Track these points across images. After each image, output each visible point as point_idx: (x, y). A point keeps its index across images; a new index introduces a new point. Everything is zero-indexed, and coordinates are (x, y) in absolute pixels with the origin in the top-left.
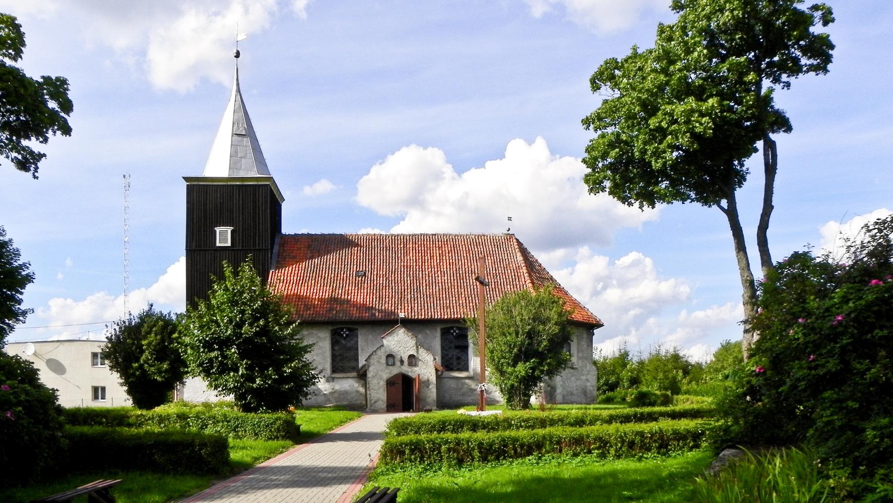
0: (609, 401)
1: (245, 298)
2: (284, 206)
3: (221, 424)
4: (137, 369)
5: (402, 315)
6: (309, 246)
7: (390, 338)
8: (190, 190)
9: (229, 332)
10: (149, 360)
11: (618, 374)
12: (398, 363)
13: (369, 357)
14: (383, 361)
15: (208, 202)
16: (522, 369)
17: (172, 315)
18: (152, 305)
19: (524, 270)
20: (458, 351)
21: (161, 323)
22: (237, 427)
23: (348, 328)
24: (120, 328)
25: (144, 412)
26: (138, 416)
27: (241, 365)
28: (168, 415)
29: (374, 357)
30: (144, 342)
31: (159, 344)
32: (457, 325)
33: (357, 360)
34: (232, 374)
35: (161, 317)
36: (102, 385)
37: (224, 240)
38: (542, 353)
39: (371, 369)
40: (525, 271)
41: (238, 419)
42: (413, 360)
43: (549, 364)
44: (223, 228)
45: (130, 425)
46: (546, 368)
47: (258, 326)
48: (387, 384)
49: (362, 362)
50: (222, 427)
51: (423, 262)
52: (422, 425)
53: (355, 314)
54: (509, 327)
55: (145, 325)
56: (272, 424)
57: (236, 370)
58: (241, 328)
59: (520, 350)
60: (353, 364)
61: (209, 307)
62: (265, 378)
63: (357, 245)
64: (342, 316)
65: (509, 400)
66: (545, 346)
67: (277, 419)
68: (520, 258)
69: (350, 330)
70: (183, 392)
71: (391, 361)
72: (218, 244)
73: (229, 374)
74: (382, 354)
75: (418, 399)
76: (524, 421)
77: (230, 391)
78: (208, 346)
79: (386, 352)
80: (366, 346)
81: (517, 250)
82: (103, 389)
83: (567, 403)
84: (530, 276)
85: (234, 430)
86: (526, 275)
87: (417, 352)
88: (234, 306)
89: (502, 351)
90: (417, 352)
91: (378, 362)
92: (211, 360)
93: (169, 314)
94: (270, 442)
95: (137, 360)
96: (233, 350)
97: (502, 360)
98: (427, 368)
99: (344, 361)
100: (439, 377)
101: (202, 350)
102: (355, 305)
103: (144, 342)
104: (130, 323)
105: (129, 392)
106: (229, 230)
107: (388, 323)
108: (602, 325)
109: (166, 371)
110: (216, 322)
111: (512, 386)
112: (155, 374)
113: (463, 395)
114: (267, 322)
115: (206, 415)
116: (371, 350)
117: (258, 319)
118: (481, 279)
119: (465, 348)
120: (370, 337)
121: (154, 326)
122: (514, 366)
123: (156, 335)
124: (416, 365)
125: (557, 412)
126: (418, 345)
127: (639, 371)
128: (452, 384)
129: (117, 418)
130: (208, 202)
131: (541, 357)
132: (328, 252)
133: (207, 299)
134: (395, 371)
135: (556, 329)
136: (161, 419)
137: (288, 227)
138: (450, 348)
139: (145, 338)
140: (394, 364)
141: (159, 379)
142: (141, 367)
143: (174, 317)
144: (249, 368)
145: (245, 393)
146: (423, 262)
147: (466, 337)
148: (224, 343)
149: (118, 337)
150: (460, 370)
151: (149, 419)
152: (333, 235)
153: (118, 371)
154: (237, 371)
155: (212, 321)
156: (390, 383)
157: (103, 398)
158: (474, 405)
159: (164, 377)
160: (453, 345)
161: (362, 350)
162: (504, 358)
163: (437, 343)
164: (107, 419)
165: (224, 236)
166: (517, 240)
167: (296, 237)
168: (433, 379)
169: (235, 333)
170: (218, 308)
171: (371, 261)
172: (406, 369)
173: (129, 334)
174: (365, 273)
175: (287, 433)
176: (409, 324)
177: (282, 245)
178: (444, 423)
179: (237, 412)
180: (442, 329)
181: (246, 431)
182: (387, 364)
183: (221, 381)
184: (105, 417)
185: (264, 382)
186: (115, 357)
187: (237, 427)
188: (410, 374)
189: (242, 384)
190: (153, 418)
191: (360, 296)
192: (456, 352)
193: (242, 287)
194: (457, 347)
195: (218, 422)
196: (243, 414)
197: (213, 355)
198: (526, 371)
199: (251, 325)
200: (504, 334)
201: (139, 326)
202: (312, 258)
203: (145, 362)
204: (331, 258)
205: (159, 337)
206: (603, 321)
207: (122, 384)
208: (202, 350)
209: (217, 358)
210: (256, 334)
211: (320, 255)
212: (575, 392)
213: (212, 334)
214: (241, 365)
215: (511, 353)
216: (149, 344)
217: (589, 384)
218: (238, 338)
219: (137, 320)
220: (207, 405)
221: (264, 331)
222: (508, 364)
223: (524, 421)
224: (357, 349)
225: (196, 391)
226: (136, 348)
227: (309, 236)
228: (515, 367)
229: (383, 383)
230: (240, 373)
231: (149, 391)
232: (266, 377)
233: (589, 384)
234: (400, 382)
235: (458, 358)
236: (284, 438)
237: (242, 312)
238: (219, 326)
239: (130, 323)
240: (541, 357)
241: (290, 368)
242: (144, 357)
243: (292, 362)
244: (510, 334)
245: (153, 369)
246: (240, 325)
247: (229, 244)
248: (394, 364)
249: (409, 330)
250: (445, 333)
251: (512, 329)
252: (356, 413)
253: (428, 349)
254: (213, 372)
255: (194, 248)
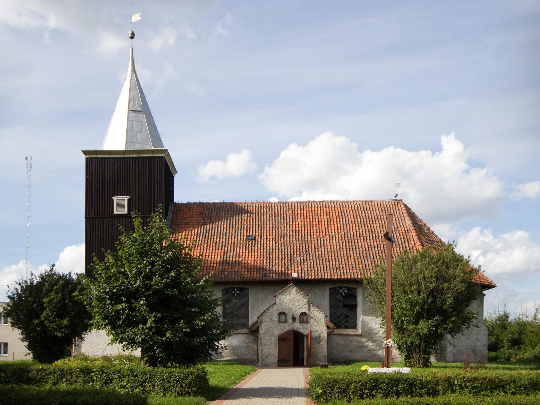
0: (492, 360)
1: (155, 249)
2: (177, 178)
3: (127, 379)
4: (37, 325)
5: (295, 275)
6: (201, 214)
7: (282, 297)
8: (89, 162)
9: (138, 284)
10: (49, 316)
11: (498, 336)
12: (290, 321)
13: (262, 314)
14: (276, 318)
15: (105, 174)
16: (423, 326)
17: (72, 274)
18: (53, 266)
19: (414, 233)
20: (346, 309)
21: (61, 282)
22: (145, 381)
23: (243, 285)
24: (22, 287)
25: (45, 366)
26: (39, 370)
27: (150, 317)
28: (71, 369)
29: (267, 314)
30: (45, 300)
31: (60, 301)
32: (347, 285)
33: (247, 318)
34: (140, 326)
35: (63, 278)
36: (5, 341)
37: (120, 208)
38: (445, 311)
39: (263, 325)
40: (414, 234)
41: (145, 373)
42: (304, 317)
43: (453, 322)
44: (120, 198)
45: (29, 381)
46: (451, 325)
47: (168, 278)
48: (279, 340)
49: (252, 319)
50: (128, 382)
51: (312, 227)
52: (352, 383)
53: (247, 276)
54: (411, 285)
55: (46, 284)
56: (183, 379)
57: (145, 322)
58: (151, 280)
59: (422, 308)
60: (243, 321)
61: (117, 258)
62: (175, 331)
63: (247, 212)
64: (234, 277)
65: (407, 358)
66: (450, 304)
67: (188, 374)
68: (408, 222)
69: (240, 289)
70: (81, 347)
71: (283, 318)
72: (115, 212)
73: (138, 326)
74: (274, 312)
75: (309, 354)
76: (469, 381)
77: (138, 344)
78: (115, 298)
79: (278, 310)
80: (257, 306)
81: (405, 215)
82: (6, 345)
83: (456, 362)
84: (419, 238)
85: (142, 385)
86: (416, 238)
87: (309, 310)
88: (143, 257)
89: (402, 308)
90: (309, 310)
91: (271, 319)
92: (118, 312)
93: (70, 274)
94: (181, 398)
95: (38, 317)
96: (142, 302)
97: (403, 318)
98: (319, 324)
99: (237, 320)
100: (329, 334)
101: (108, 302)
102: (246, 266)
103: (45, 300)
104: (32, 283)
105: (29, 347)
106: (126, 198)
107: (283, 283)
108: (494, 286)
109: (66, 327)
110: (124, 273)
111: (412, 343)
112: (55, 330)
113: (351, 351)
114: (179, 274)
115: (107, 369)
116: (261, 309)
117: (170, 270)
118: (390, 235)
119: (354, 307)
120: (261, 296)
121: (55, 284)
122: (416, 322)
123: (57, 293)
124: (307, 322)
125: (484, 371)
126: (309, 304)
127: (521, 333)
128: (340, 341)
129: (18, 372)
130: (105, 174)
131: (445, 315)
132: (220, 219)
133: (115, 250)
134: (287, 327)
135: (462, 287)
136: (64, 373)
137: (181, 196)
138: (338, 307)
139: (46, 296)
140: (286, 321)
141: (59, 334)
142: (42, 323)
143: (75, 277)
144: (158, 321)
145: (153, 346)
146: (312, 227)
147: (355, 297)
148: (132, 295)
149: (19, 296)
150: (347, 327)
151: (50, 373)
152: (224, 203)
153: (19, 328)
154: (145, 323)
155: (120, 273)
156: (282, 339)
157: (5, 352)
158: (380, 361)
159: (64, 332)
160: (341, 304)
161: (253, 308)
162: (405, 315)
163: (326, 302)
164: (6, 374)
165: (121, 204)
166: (404, 204)
167: (189, 206)
168: (324, 335)
169: (144, 286)
170: (126, 259)
171: (261, 227)
172: (297, 326)
173: (31, 293)
174: (255, 238)
175: (199, 389)
176: (301, 283)
177: (175, 213)
178: (376, 380)
179: (143, 367)
180: (330, 289)
181: (154, 386)
182: (279, 321)
183: (125, 336)
184: (4, 371)
185: (175, 335)
186: (17, 314)
187: (145, 381)
188: (301, 331)
189: (151, 337)
190: (55, 373)
191: (251, 258)
192: (344, 311)
193: (152, 238)
194: (345, 306)
195: (124, 376)
196: (151, 368)
197: (120, 307)
198: (429, 329)
199: (161, 276)
200: (405, 292)
201: (40, 285)
202: (204, 224)
203: (46, 319)
204: (223, 224)
205: (59, 295)
206: (495, 282)
207: (23, 340)
208: (108, 302)
209: (124, 310)
210: (167, 285)
211: (211, 222)
212: (465, 351)
213: (120, 285)
214: (150, 317)
215: (413, 310)
216: (50, 302)
217: (479, 344)
218: (148, 290)
219: (39, 279)
220: (107, 359)
221: (175, 283)
222: (409, 322)
223: (469, 381)
224: (247, 307)
225: (98, 344)
226: (37, 306)
227: (201, 204)
228: (416, 325)
229: (274, 339)
230: (148, 325)
231: (50, 344)
232: (176, 330)
233: (479, 344)
234: (292, 338)
235: (347, 317)
236: (195, 394)
237: (152, 263)
238: (127, 277)
239: (32, 283)
240: (445, 315)
241: (203, 320)
242: (44, 314)
243: (204, 315)
244: (412, 292)
245: (53, 325)
246: (149, 277)
247: (126, 212)
248: (286, 321)
249: (301, 289)
250: (333, 293)
251: (415, 287)
252: (251, 367)
253: (319, 307)
254: (119, 327)
255: (93, 215)
